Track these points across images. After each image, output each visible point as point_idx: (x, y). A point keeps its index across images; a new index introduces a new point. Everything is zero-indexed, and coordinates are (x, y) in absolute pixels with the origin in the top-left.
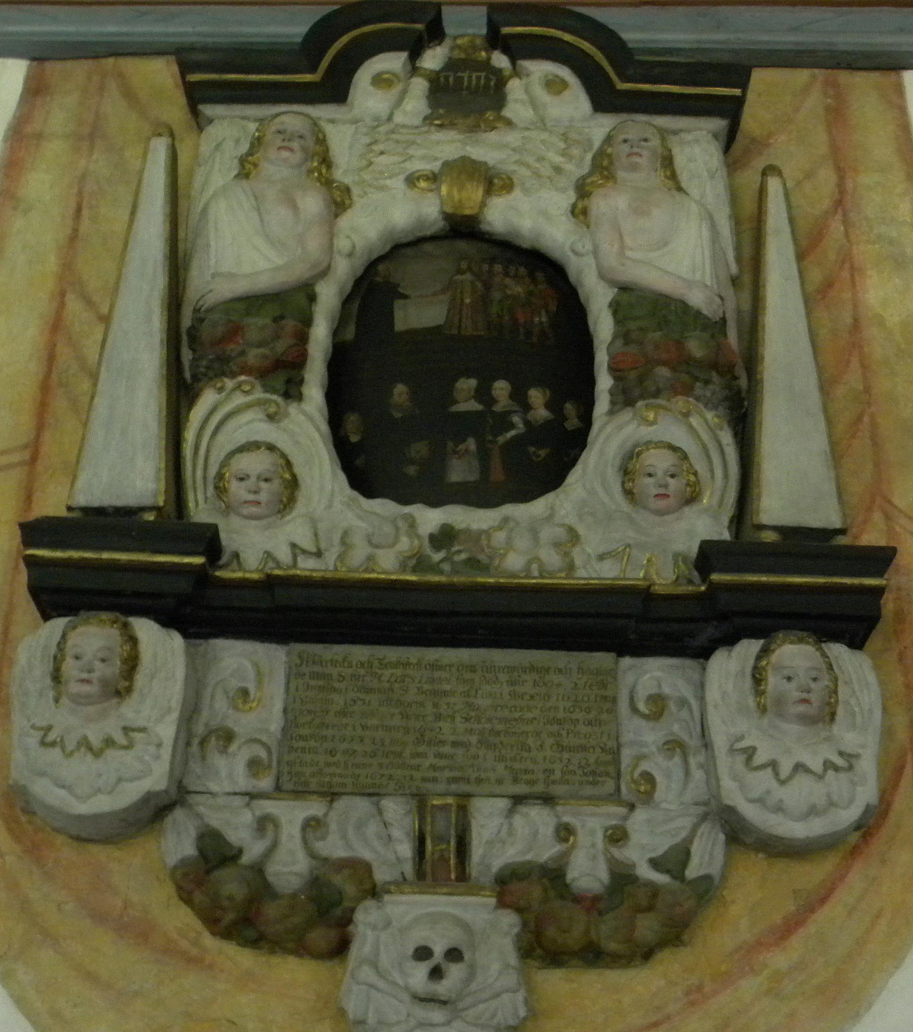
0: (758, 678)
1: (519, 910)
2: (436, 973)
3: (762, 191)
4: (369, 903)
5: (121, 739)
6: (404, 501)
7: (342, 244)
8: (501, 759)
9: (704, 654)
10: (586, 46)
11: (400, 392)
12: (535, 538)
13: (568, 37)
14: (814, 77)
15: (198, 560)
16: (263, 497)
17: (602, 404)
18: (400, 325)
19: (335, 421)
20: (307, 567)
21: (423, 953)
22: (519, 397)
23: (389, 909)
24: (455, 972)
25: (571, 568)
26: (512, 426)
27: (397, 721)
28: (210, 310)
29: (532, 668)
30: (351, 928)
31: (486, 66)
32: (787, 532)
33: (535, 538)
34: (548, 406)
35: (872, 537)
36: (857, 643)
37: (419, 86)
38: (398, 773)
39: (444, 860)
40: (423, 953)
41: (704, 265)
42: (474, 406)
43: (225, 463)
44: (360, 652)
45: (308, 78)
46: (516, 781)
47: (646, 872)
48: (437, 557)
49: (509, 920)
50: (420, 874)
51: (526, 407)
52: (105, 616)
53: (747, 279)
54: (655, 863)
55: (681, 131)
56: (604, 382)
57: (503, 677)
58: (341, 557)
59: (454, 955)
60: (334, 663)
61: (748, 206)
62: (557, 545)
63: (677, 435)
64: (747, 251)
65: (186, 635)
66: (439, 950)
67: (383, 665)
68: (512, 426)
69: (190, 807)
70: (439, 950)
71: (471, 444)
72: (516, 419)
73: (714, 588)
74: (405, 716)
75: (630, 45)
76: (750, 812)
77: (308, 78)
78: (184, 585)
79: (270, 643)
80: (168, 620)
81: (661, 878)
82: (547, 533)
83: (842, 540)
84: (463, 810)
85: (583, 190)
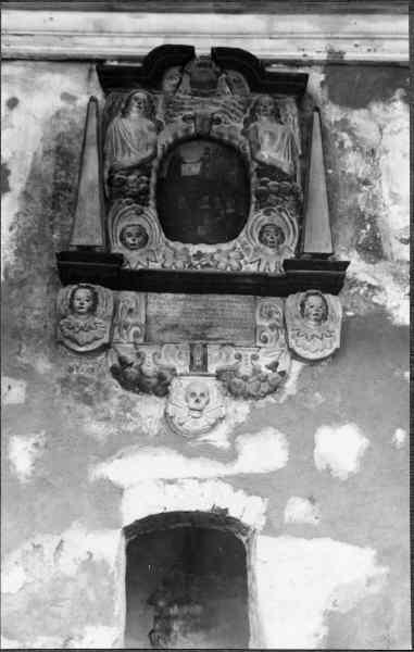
0: (303, 305)
2: (197, 401)
5: (93, 326)
6: (184, 242)
9: (287, 296)
12: (229, 258)
16: (136, 242)
17: (253, 207)
18: (183, 174)
30: (169, 388)
36: (336, 293)
49: (220, 384)
54: (269, 367)
66: (198, 394)
69: (370, 109)
70: (198, 394)
79: (197, 512)
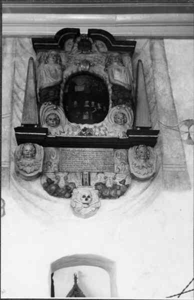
1: (99, 190)
2: (86, 200)
3: (138, 64)
4: (75, 189)
6: (78, 123)
7: (65, 77)
8: (95, 166)
9: (128, 148)
10: (107, 38)
11: (75, 103)
12: (100, 130)
13: (103, 36)
14: (148, 41)
15: (45, 134)
19: (64, 108)
20: (63, 135)
21: (84, 196)
22: (96, 104)
23: (79, 190)
24: (89, 199)
25: (106, 135)
26: (94, 110)
27: (78, 160)
28: (43, 90)
29: (100, 151)
31: (88, 41)
32: (141, 128)
33: (100, 130)
34: (101, 107)
35: (155, 128)
37: (76, 45)
38: (79, 169)
39: (86, 182)
40: (84, 196)
41: (123, 143)
42: (88, 106)
43: (47, 117)
44: (71, 149)
45: (56, 44)
46: (98, 170)
47: (118, 184)
48: (84, 133)
50: (83, 185)
51: (97, 107)
52: (31, 144)
53: (135, 81)
55: (129, 164)
56: (111, 101)
57: (95, 153)
58: (68, 133)
59: (89, 197)
60: (68, 151)
61: (135, 67)
62: (104, 131)
63: (123, 111)
64: (135, 76)
65: (43, 146)
67: (76, 151)
68: (94, 110)
71: (87, 113)
72: (95, 109)
73: (130, 137)
74: (79, 159)
75: (114, 35)
76: (135, 174)
77: (56, 44)
78: (43, 138)
80: (40, 144)
81: (121, 185)
82: (102, 128)
83: (151, 129)
84: (89, 175)
85: (106, 66)
